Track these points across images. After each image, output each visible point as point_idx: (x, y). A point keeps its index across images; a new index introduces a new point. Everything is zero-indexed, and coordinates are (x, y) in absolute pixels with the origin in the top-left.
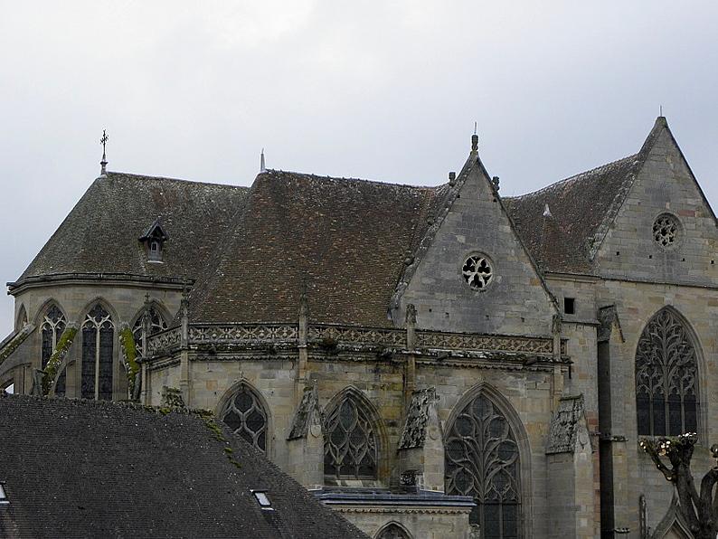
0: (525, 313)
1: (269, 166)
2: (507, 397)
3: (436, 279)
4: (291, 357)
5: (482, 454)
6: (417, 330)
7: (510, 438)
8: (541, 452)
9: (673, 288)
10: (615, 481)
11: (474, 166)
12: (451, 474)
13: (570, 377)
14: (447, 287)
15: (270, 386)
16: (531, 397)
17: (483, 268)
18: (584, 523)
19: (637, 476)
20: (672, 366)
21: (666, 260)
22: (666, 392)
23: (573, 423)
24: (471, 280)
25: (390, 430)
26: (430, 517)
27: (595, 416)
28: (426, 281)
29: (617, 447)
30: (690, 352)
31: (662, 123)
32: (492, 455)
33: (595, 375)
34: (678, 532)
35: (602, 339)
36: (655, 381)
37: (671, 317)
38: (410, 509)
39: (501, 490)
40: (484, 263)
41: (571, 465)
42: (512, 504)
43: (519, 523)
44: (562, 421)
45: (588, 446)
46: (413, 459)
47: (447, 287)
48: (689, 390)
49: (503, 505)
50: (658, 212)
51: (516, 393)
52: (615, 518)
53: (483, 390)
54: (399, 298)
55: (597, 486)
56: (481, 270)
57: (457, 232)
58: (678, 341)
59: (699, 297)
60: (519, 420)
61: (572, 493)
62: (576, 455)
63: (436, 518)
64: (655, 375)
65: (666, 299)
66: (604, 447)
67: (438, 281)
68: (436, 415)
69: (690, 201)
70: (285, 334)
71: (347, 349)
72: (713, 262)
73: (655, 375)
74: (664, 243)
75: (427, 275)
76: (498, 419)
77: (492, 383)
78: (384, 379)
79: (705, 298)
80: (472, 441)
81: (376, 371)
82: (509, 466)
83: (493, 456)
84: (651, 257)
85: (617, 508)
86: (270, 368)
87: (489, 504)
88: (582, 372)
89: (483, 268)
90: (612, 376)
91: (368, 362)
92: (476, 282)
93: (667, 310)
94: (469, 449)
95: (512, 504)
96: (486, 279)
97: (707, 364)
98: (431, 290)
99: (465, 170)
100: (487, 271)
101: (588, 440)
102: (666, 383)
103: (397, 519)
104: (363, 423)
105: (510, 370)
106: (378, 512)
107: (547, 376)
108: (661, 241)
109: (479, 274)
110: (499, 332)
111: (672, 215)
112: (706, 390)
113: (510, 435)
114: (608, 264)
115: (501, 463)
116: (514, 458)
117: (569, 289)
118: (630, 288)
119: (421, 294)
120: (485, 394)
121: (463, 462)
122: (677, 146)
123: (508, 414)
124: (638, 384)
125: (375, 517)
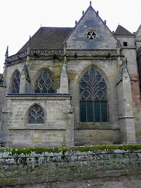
8: (114, 84)
11: (91, 7)
13: (127, 64)
16: (110, 68)
18: (128, 105)
24: (89, 38)
26: (52, 101)
33: (136, 63)
38: (42, 98)
40: (94, 33)
41: (122, 86)
42: (105, 102)
43: (108, 108)
47: (80, 39)
49: (101, 102)
51: (105, 67)
53: (92, 67)
56: (92, 35)
57: (84, 25)
60: (105, 75)
61: (123, 95)
63: (55, 102)
67: (78, 38)
71: (42, 56)
75: (74, 36)
77: (95, 64)
78: (56, 64)
80: (89, 82)
81: (54, 62)
87: (96, 102)
88: (131, 62)
91: (51, 59)
94: (88, 84)
95: (105, 102)
96: (95, 37)
98: (75, 40)
103: (38, 102)
105: (101, 60)
116: (105, 87)
119: (72, 41)
120: (93, 67)
123: (102, 73)
125: (28, 101)
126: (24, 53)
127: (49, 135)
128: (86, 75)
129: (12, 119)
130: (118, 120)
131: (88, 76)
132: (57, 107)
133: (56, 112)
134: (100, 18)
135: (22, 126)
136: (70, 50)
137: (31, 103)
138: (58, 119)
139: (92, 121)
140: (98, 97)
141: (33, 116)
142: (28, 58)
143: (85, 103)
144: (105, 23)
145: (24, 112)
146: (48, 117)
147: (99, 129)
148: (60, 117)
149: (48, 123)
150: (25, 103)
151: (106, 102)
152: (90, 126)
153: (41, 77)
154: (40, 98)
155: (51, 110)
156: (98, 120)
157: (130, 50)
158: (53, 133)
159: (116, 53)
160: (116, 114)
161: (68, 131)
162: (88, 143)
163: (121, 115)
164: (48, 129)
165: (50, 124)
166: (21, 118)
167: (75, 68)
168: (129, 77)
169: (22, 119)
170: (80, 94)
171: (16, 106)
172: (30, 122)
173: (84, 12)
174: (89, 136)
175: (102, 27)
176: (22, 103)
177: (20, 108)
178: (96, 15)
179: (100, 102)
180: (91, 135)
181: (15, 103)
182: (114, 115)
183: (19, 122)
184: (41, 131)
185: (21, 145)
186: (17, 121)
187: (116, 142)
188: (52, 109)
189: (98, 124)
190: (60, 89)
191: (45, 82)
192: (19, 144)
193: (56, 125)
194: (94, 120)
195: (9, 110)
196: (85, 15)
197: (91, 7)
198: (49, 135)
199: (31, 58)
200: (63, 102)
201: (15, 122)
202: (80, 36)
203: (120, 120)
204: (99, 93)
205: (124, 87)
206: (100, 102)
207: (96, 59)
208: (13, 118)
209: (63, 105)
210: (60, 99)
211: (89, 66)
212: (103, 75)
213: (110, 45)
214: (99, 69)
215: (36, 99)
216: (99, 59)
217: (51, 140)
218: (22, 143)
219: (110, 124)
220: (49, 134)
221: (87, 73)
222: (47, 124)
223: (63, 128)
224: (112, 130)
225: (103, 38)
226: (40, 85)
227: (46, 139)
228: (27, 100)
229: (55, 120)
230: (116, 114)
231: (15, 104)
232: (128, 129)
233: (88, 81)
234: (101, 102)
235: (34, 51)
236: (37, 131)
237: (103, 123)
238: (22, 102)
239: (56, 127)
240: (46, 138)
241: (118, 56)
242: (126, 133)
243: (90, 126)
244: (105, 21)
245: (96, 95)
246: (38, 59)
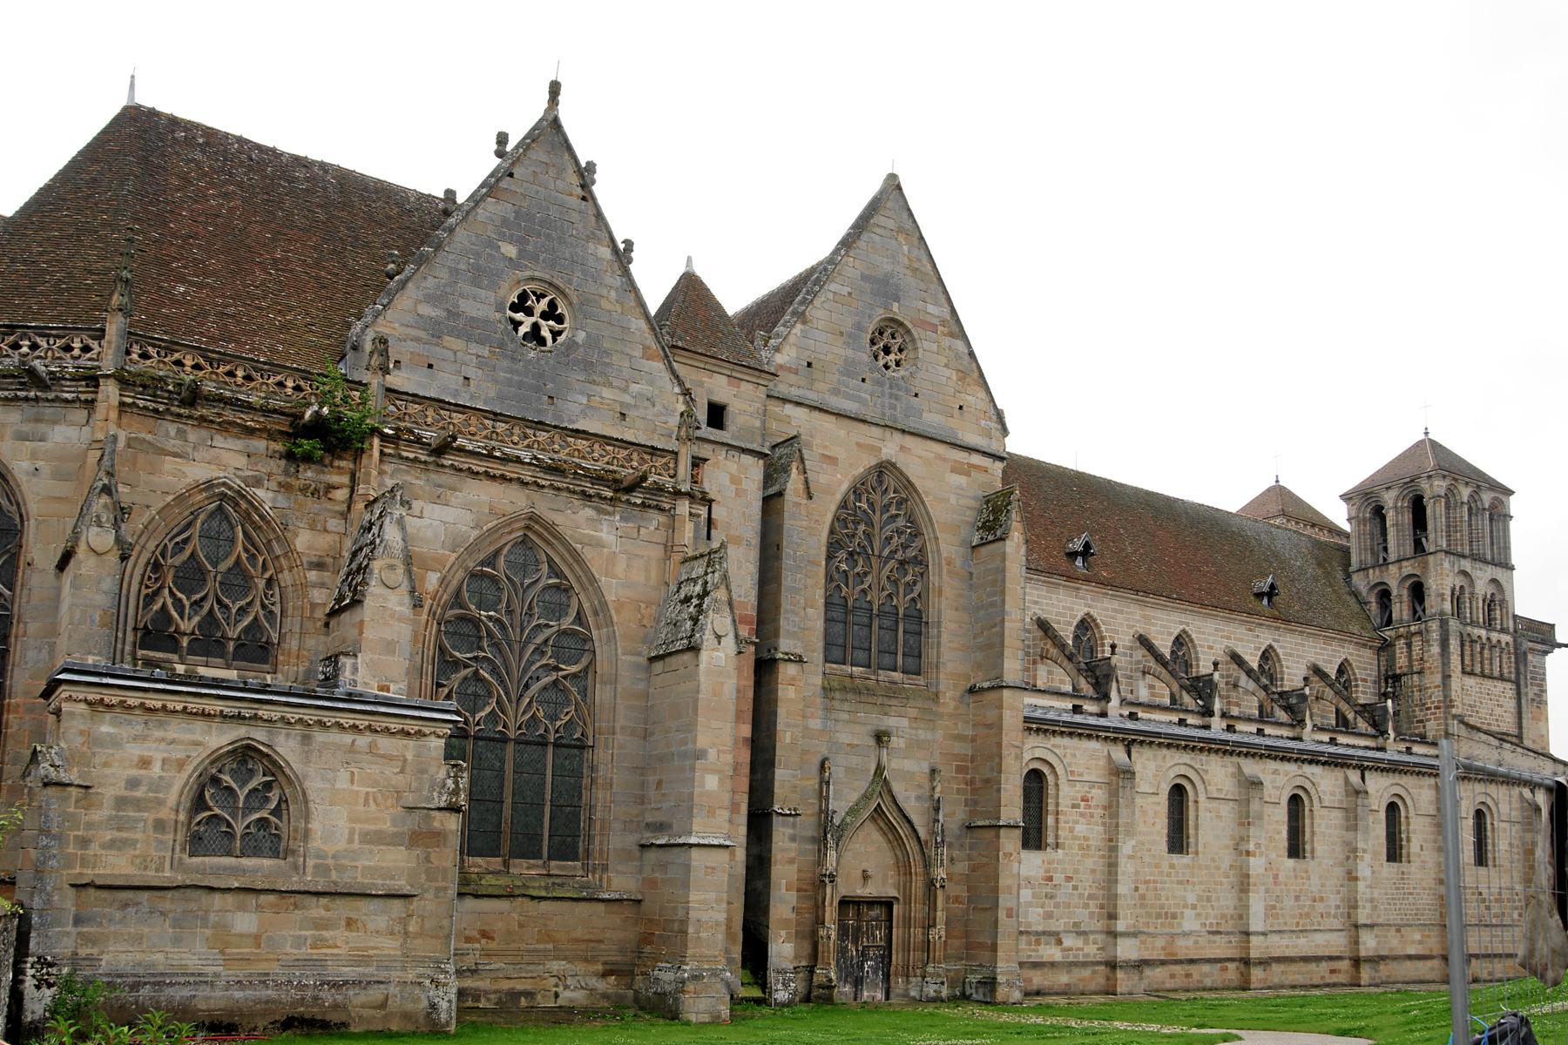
0: (628, 406)
1: (146, 99)
2: (578, 547)
3: (449, 311)
4: (83, 397)
5: (516, 647)
6: (389, 390)
7: (581, 625)
8: (639, 654)
9: (897, 436)
10: (780, 727)
11: (549, 131)
12: (448, 679)
14: (472, 330)
15: (34, 456)
17: (551, 314)
18: (711, 782)
19: (819, 726)
20: (889, 558)
21: (887, 391)
22: (876, 598)
23: (701, 597)
24: (523, 330)
25: (313, 575)
26: (347, 738)
27: (752, 612)
28: (426, 310)
29: (787, 671)
30: (917, 543)
31: (893, 186)
32: (540, 651)
34: (882, 825)
35: (771, 491)
36: (861, 577)
37: (890, 481)
38: (293, 715)
39: (553, 718)
40: (552, 305)
41: (693, 676)
42: (575, 747)
43: (586, 781)
44: (682, 596)
45: (729, 643)
47: (472, 330)
48: (913, 599)
49: (556, 745)
50: (880, 314)
51: (600, 544)
52: (776, 790)
53: (527, 527)
54: (363, 330)
55: (746, 730)
56: (544, 316)
57: (503, 237)
58: (901, 522)
59: (939, 457)
61: (691, 727)
62: (704, 655)
63: (363, 741)
64: (858, 569)
65: (884, 450)
66: (764, 668)
67: (453, 314)
68: (399, 538)
69: (931, 309)
70: (76, 352)
72: (961, 408)
73: (858, 569)
74: (886, 367)
75: (431, 299)
76: (557, 587)
77: (550, 516)
79: (945, 460)
80: (498, 621)
81: (290, 456)
82: (575, 676)
83: (543, 653)
84: (863, 380)
85: (781, 775)
86: (38, 420)
87: (527, 743)
89: (551, 314)
90: (787, 551)
91: (271, 436)
92: (535, 335)
93: (884, 469)
94: (490, 634)
95: (575, 747)
96: (556, 334)
97: (944, 562)
98: (436, 330)
99: (532, 138)
100: (560, 319)
101: (730, 628)
102: (876, 585)
103: (259, 734)
104: (252, 558)
105: (586, 496)
106: (204, 715)
107: (662, 518)
108: (881, 363)
109: (542, 322)
110: (575, 426)
111: (901, 324)
112: (939, 603)
113: (579, 618)
114: (792, 378)
115: (557, 669)
116: (584, 661)
117: (718, 387)
118: (828, 422)
121: (476, 658)
122: (915, 221)
123: (578, 579)
124: (829, 578)
125: (200, 725)
126: (61, 337)
127: (320, 925)
128: (484, 575)
129: (90, 825)
130: (637, 853)
131: (494, 580)
132: (374, 769)
133: (361, 801)
134: (599, 215)
135: (157, 870)
136: (405, 397)
137: (220, 738)
138: (375, 838)
139: (493, 852)
140: (541, 714)
141: (217, 811)
142: (110, 392)
143: (463, 742)
144: (623, 256)
145: (170, 786)
146: (315, 825)
147: (533, 898)
148: (387, 826)
149: (318, 857)
150: (177, 730)
151: (582, 747)
152: (483, 882)
153: (186, 541)
154: (279, 715)
155: (338, 786)
156: (527, 848)
157: (736, 459)
158: (342, 908)
159: (672, 472)
160: (632, 821)
161: (426, 905)
162: (469, 970)
163: (660, 827)
164: (320, 888)
165: (330, 862)
166: (150, 822)
167: (426, 521)
168: (731, 636)
169: (160, 825)
170: (440, 685)
171: (116, 743)
172: (196, 844)
173: (509, 148)
174: (475, 934)
175: (608, 279)
176: (158, 734)
177: (145, 763)
178: (579, 191)
179: (550, 749)
180: (487, 928)
181: (112, 724)
182: (617, 825)
183: (136, 841)
184: (272, 898)
185: (153, 975)
186: (127, 839)
187: (614, 967)
188: (342, 782)
189: (524, 869)
190: (359, 660)
191: (219, 578)
192: (141, 971)
193: (364, 868)
194: (505, 848)
195: (75, 769)
196: (517, 171)
197: (549, 131)
198: (320, 925)
199: (129, 400)
200: (409, 748)
201: (111, 845)
202: (469, 308)
203: (652, 855)
204: (546, 695)
205: (703, 687)
206: (550, 749)
207: (559, 489)
208: (97, 815)
209: (405, 760)
210: (392, 726)
211: (509, 524)
212: (584, 589)
213: (641, 413)
214: (568, 551)
215: (255, 717)
216: (574, 492)
217: (329, 951)
218: (153, 965)
219: (594, 873)
220: (321, 919)
221: (491, 561)
222: (311, 863)
223: (402, 885)
224: (601, 907)
225: (607, 353)
226: (180, 595)
227: (299, 942)
228: (196, 714)
229: (357, 841)
230: (632, 821)
231: (111, 730)
232: (697, 902)
233: (492, 613)
234: (556, 745)
235: (154, 346)
236: (251, 900)
237: (553, 863)
238: (161, 724)
239: (361, 881)
240: (299, 937)
241: (677, 494)
242: (684, 922)
243: (483, 882)
244: (629, 244)
245: (530, 703)
246: (179, 415)
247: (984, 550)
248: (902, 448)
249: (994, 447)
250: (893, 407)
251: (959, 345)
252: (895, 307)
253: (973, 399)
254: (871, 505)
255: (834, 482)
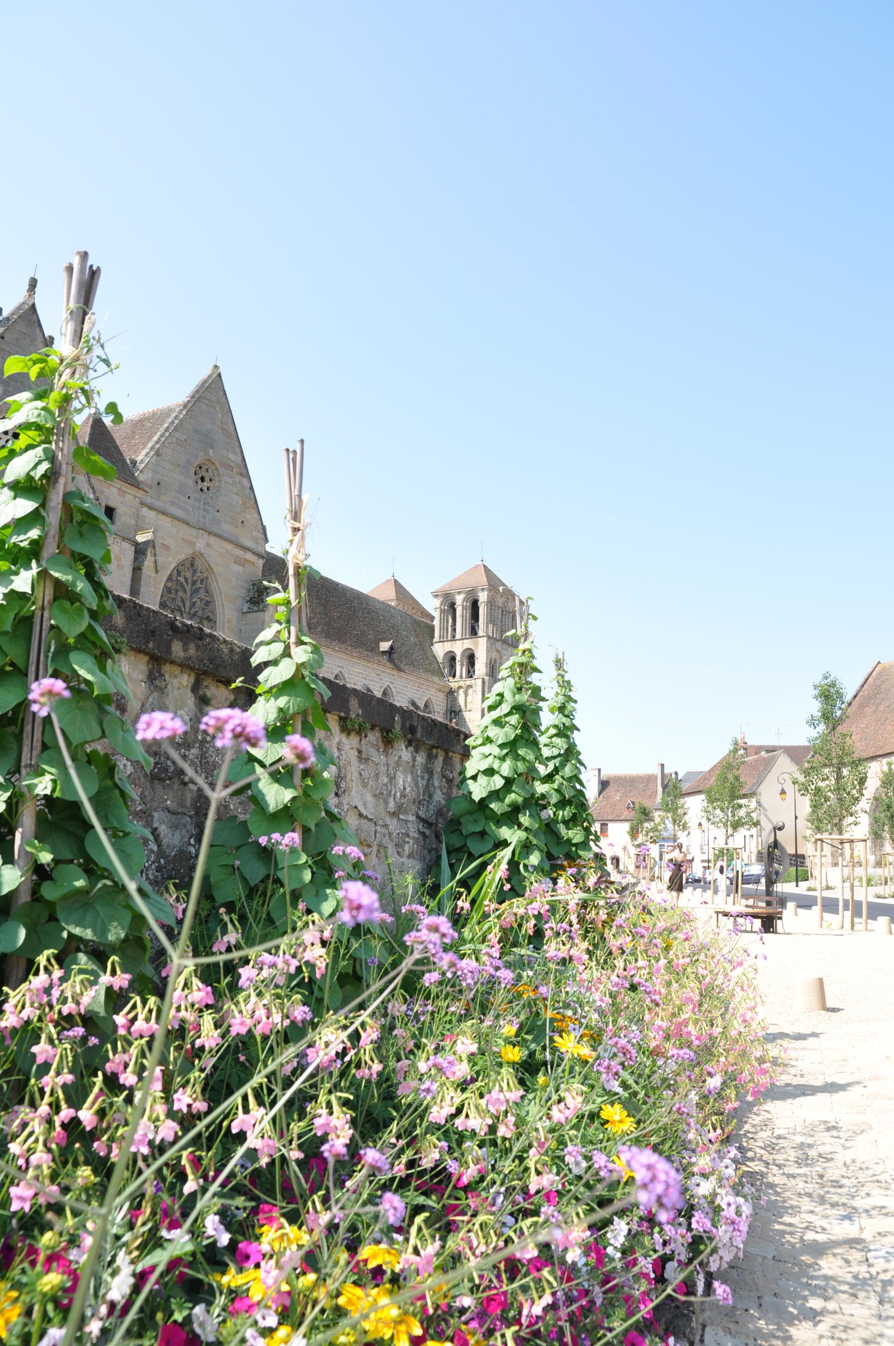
21: (202, 506)
46: (234, 757)
59: (227, 552)
69: (231, 456)
247: (250, 615)
248: (208, 544)
249: (259, 549)
250: (205, 517)
251: (245, 481)
252: (211, 452)
253: (250, 516)
254: (186, 579)
255: (169, 562)
